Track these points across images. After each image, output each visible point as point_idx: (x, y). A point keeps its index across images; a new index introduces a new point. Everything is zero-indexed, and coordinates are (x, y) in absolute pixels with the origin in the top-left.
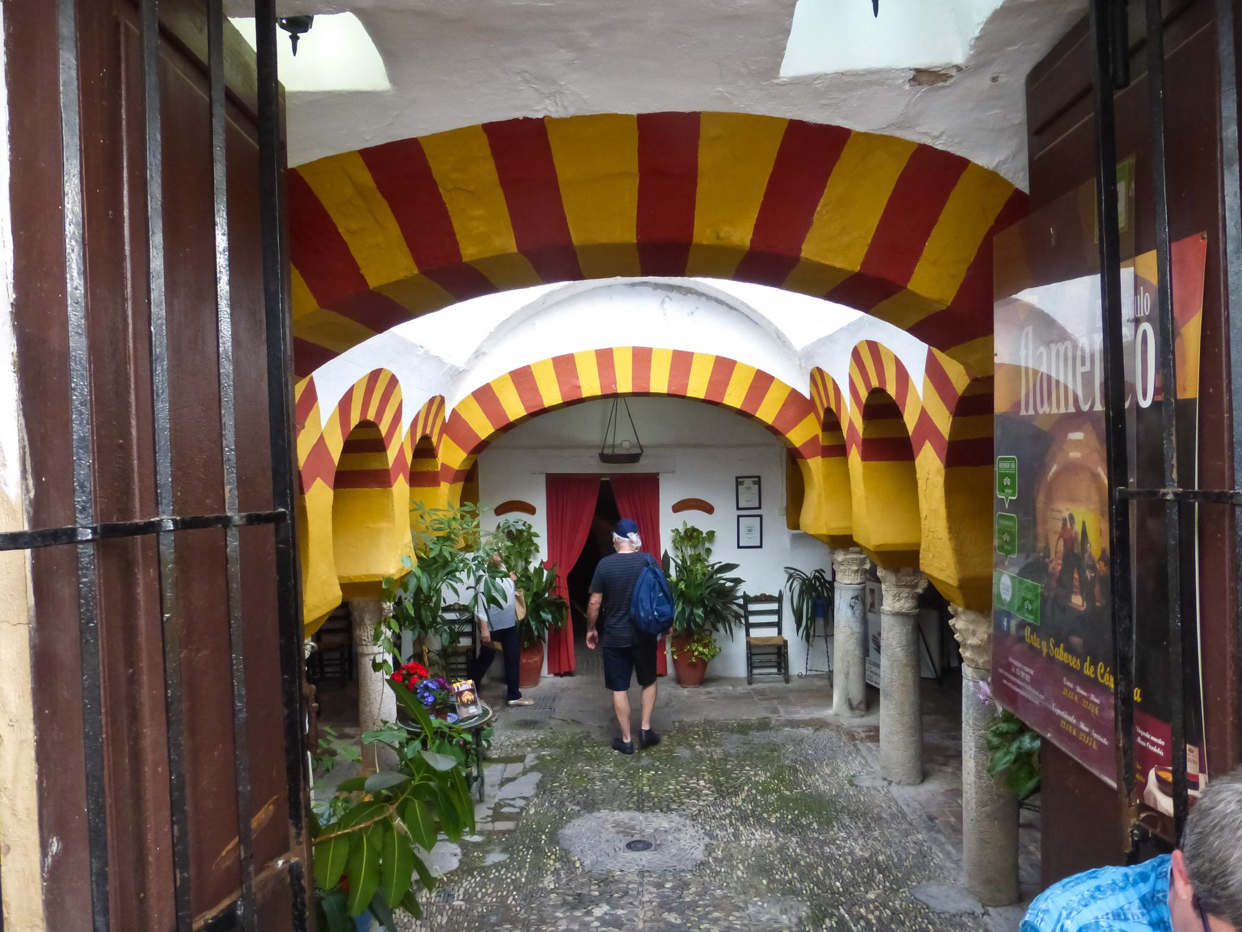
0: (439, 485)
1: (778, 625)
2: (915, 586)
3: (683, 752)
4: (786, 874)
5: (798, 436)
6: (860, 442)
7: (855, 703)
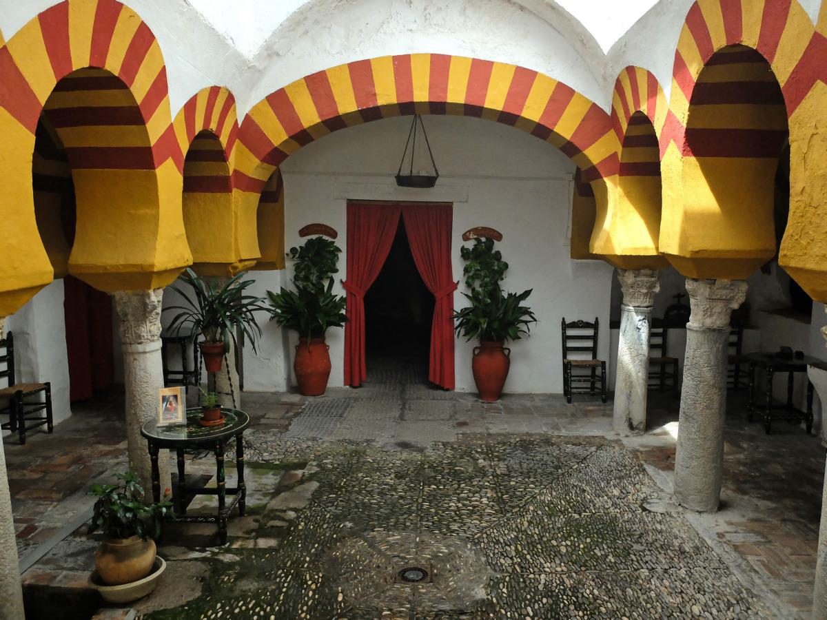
0: (231, 192)
2: (729, 301)
5: (596, 153)
6: (681, 134)
7: (635, 423)
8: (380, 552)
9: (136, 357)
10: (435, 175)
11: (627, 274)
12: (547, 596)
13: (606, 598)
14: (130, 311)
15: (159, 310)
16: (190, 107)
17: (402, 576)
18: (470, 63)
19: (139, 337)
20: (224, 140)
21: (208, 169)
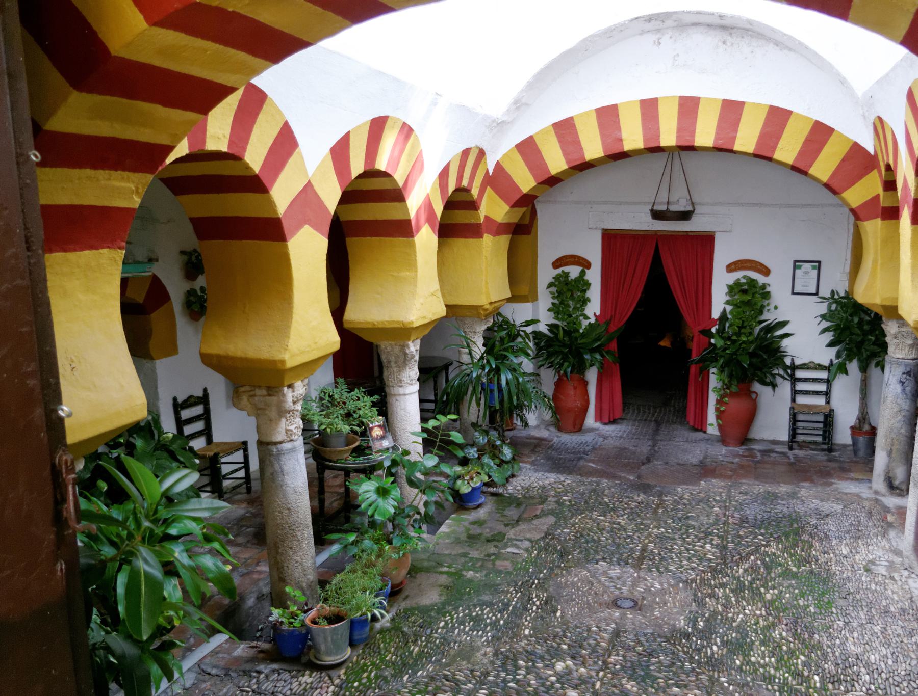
1: (827, 394)
3: (210, 588)
4: (763, 658)
6: (911, 202)
8: (599, 582)
9: (398, 398)
10: (690, 208)
12: (738, 632)
13: (791, 639)
14: (393, 359)
15: (417, 358)
16: (444, 175)
17: (615, 604)
18: (720, 104)
19: (401, 381)
20: (475, 192)
21: (462, 217)
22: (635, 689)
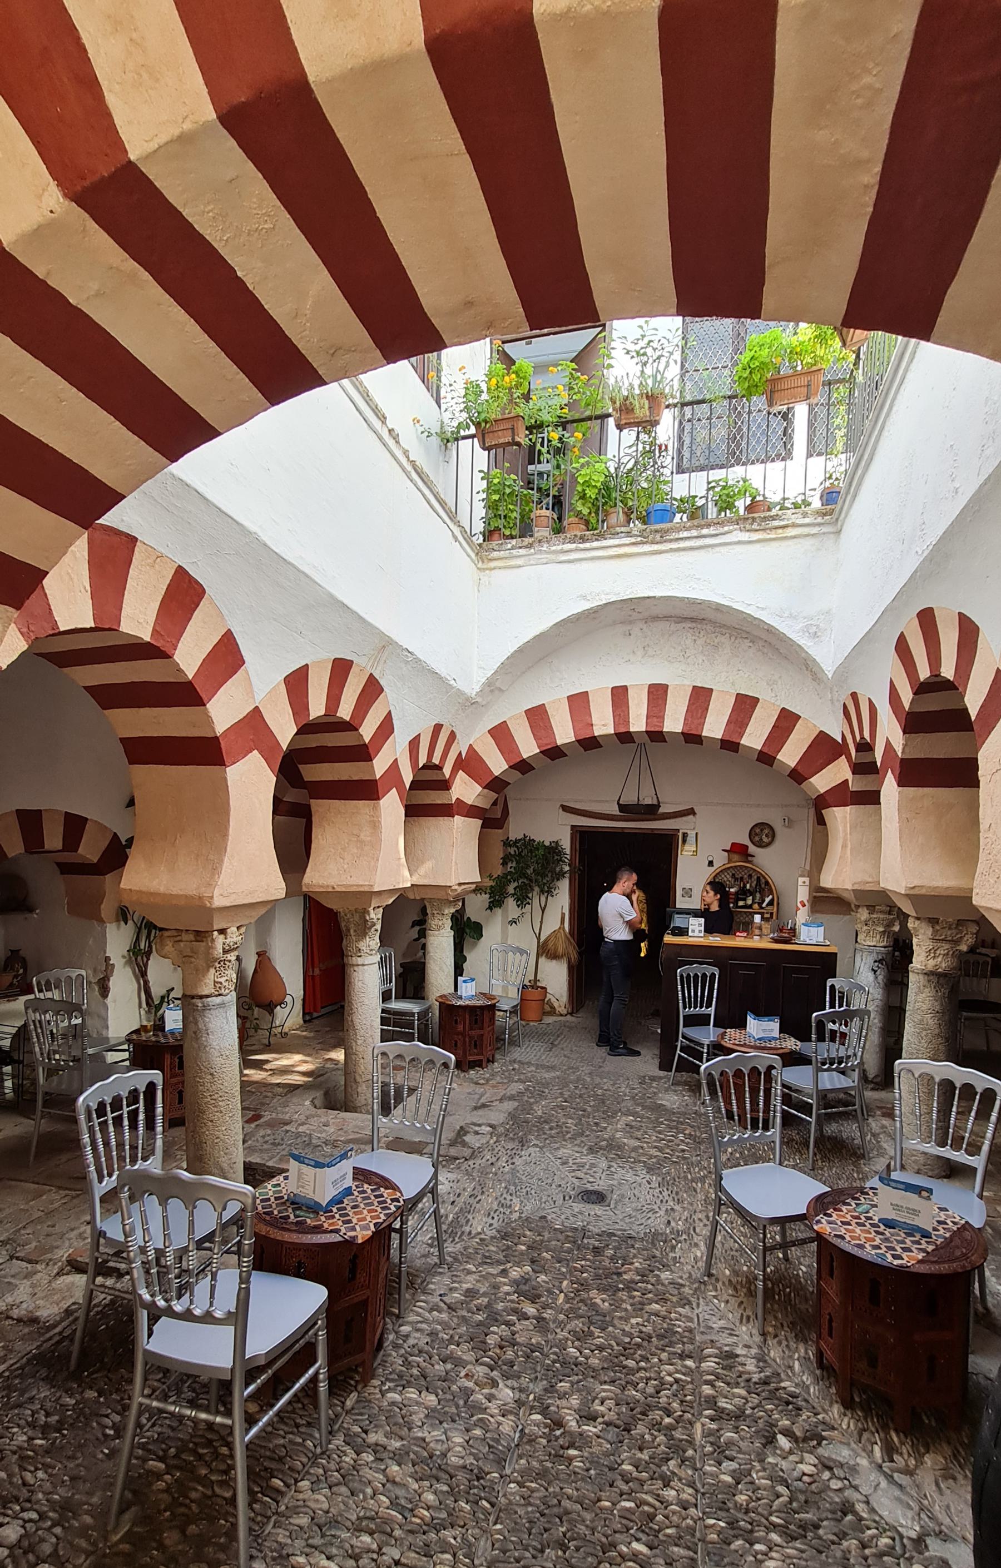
2: (957, 942)
9: (356, 968)
10: (655, 802)
11: (860, 910)
15: (378, 927)
16: (414, 744)
20: (447, 771)
22: (606, 1304)
